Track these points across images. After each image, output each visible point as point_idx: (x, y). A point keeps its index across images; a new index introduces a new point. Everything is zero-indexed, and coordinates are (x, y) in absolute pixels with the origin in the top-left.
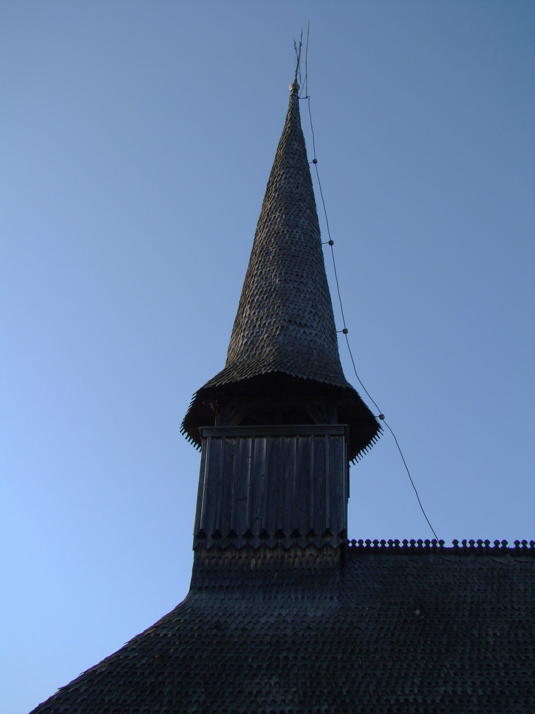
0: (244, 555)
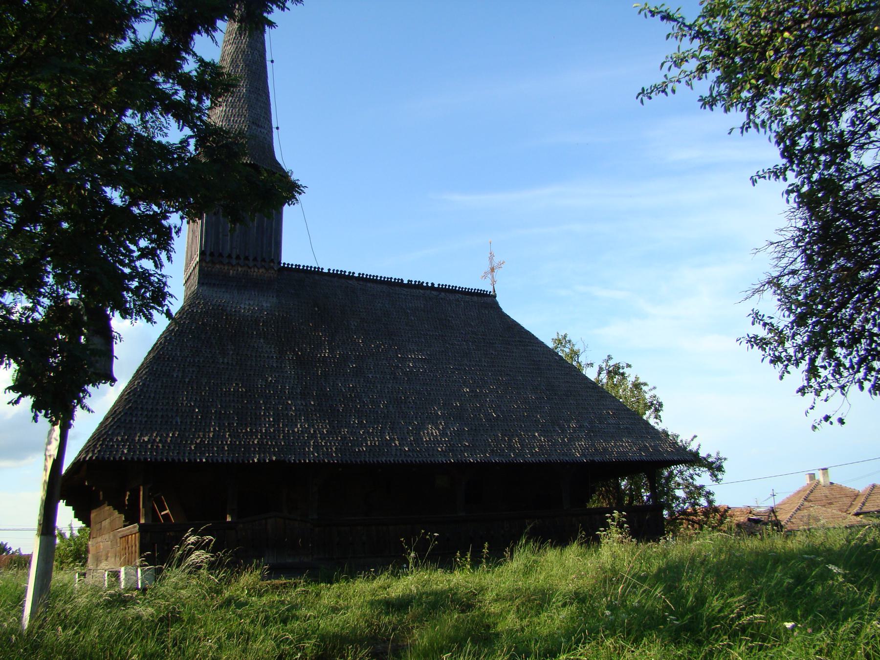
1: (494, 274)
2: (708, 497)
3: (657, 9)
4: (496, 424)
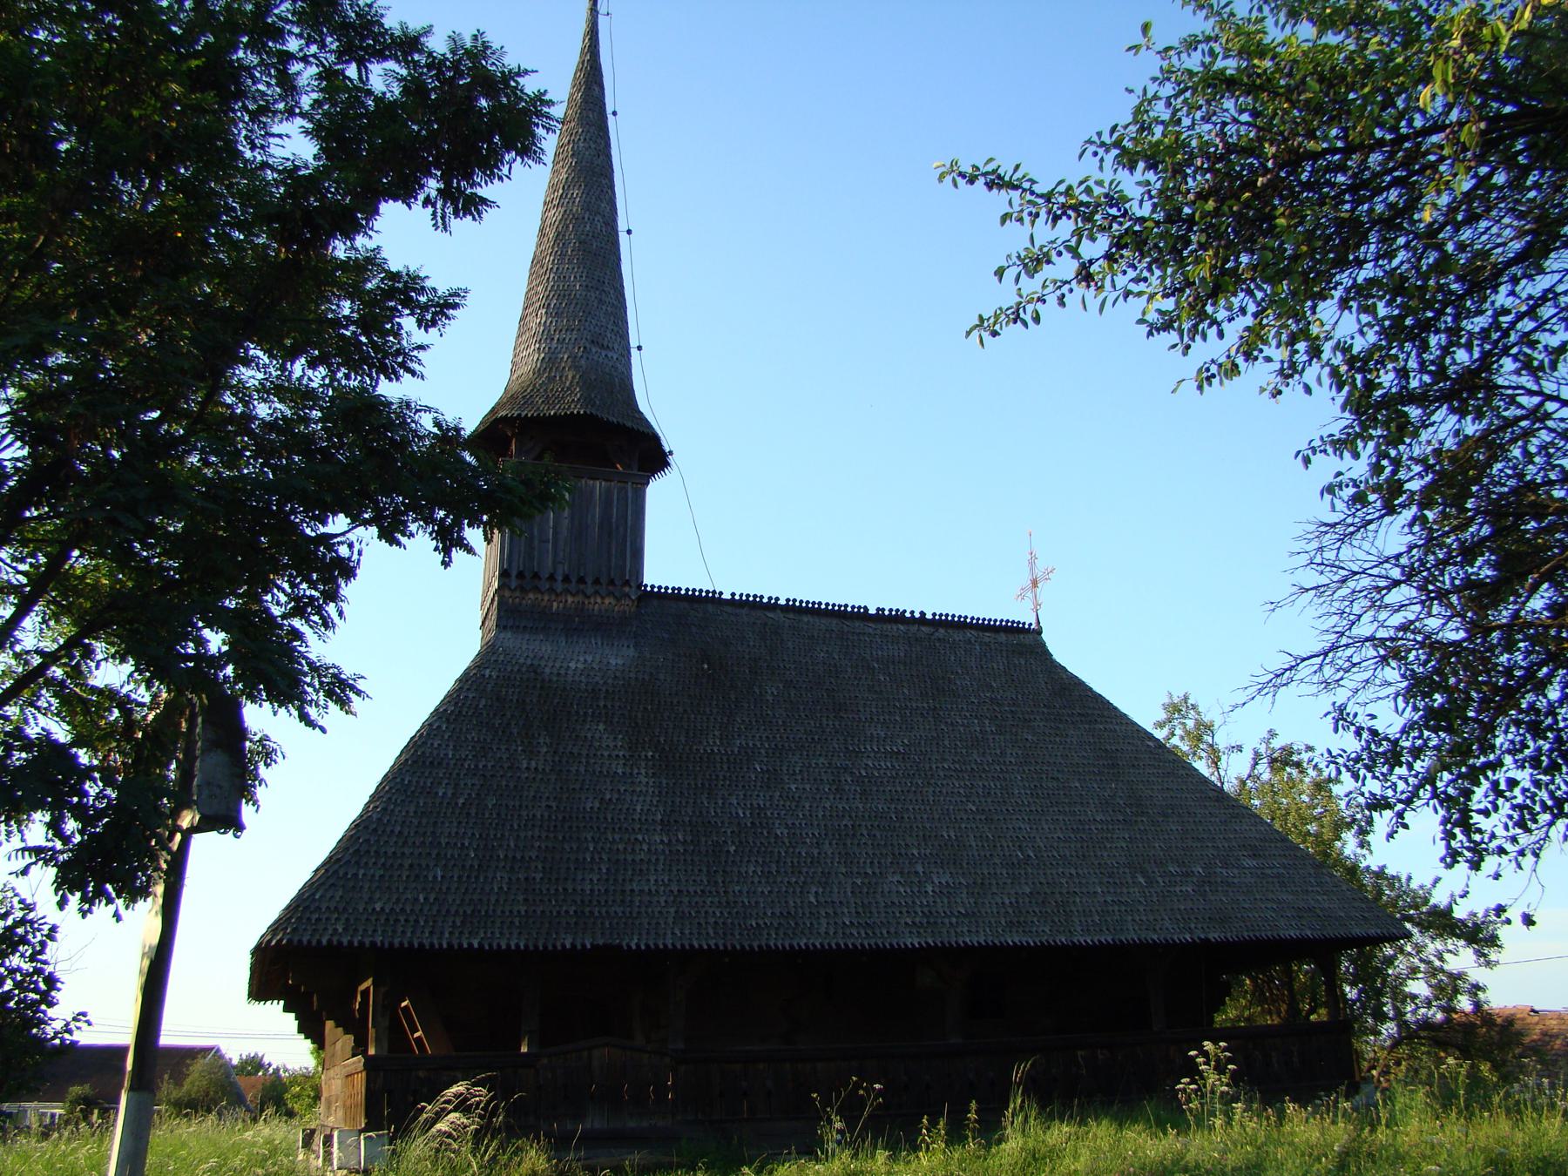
1: (1038, 590)
2: (1476, 995)
3: (978, 169)
4: (1023, 872)
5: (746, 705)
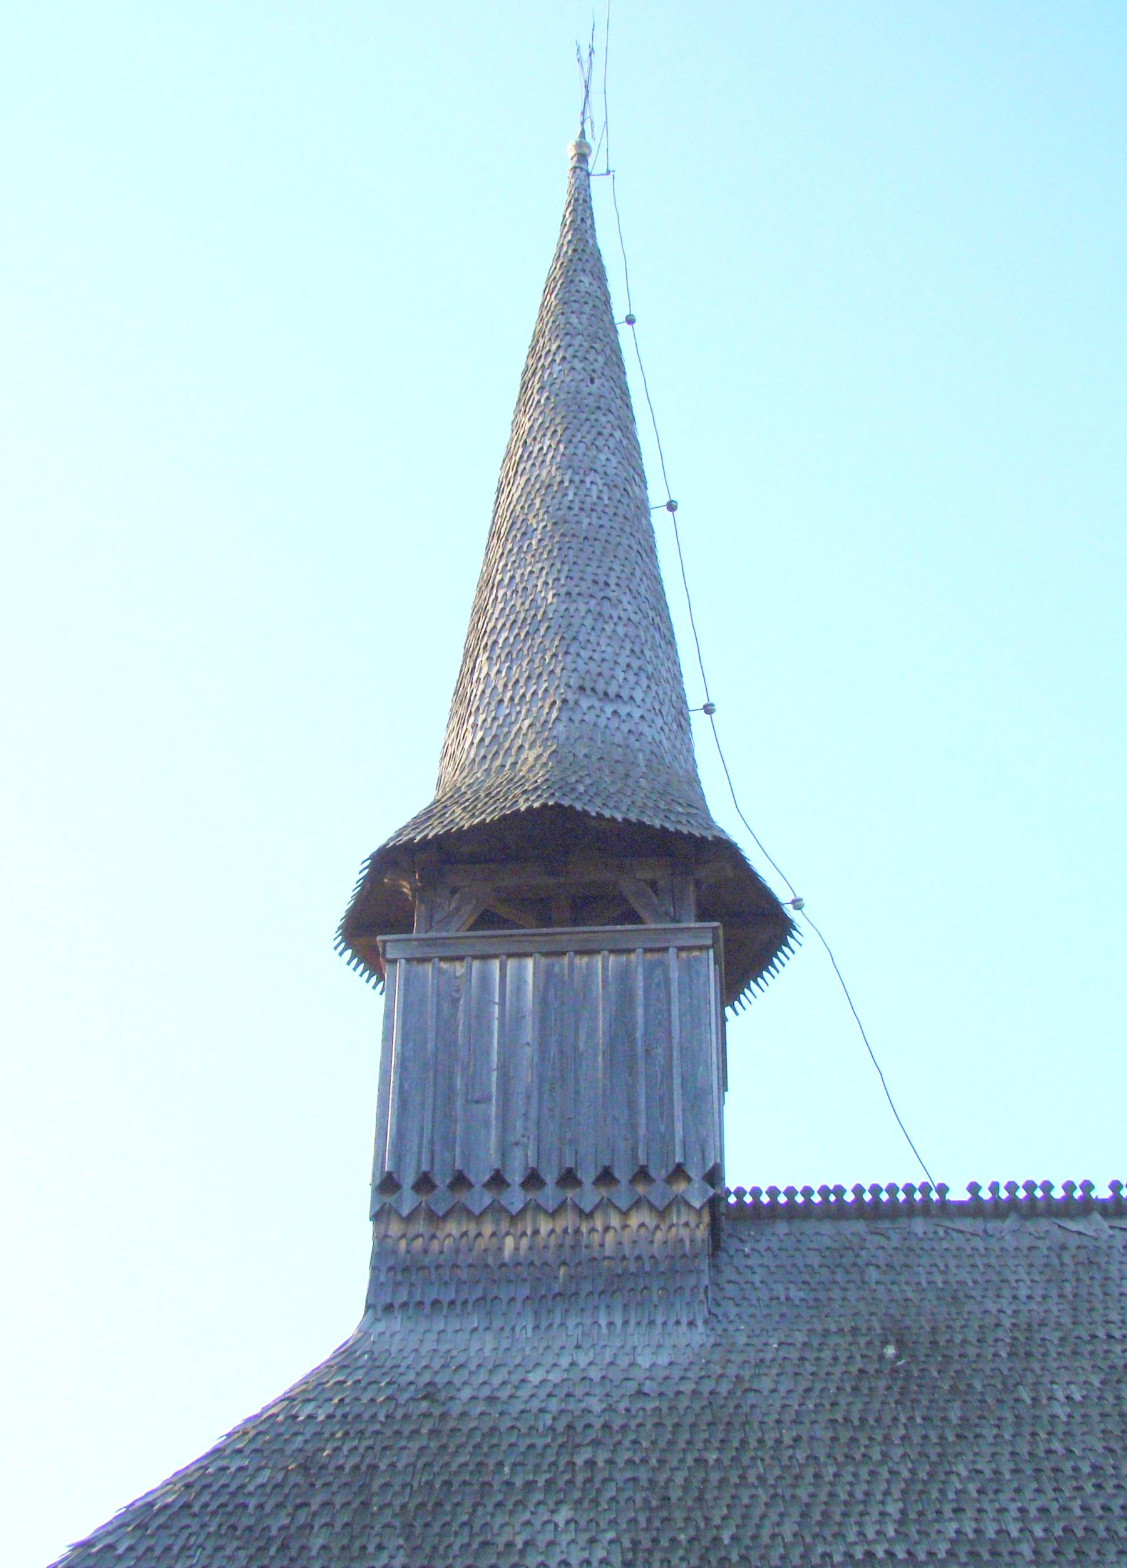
0: (488, 1229)
5: (989, 1433)
